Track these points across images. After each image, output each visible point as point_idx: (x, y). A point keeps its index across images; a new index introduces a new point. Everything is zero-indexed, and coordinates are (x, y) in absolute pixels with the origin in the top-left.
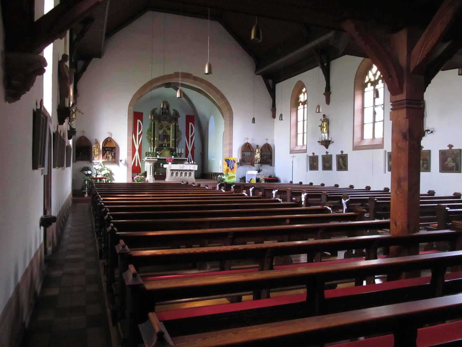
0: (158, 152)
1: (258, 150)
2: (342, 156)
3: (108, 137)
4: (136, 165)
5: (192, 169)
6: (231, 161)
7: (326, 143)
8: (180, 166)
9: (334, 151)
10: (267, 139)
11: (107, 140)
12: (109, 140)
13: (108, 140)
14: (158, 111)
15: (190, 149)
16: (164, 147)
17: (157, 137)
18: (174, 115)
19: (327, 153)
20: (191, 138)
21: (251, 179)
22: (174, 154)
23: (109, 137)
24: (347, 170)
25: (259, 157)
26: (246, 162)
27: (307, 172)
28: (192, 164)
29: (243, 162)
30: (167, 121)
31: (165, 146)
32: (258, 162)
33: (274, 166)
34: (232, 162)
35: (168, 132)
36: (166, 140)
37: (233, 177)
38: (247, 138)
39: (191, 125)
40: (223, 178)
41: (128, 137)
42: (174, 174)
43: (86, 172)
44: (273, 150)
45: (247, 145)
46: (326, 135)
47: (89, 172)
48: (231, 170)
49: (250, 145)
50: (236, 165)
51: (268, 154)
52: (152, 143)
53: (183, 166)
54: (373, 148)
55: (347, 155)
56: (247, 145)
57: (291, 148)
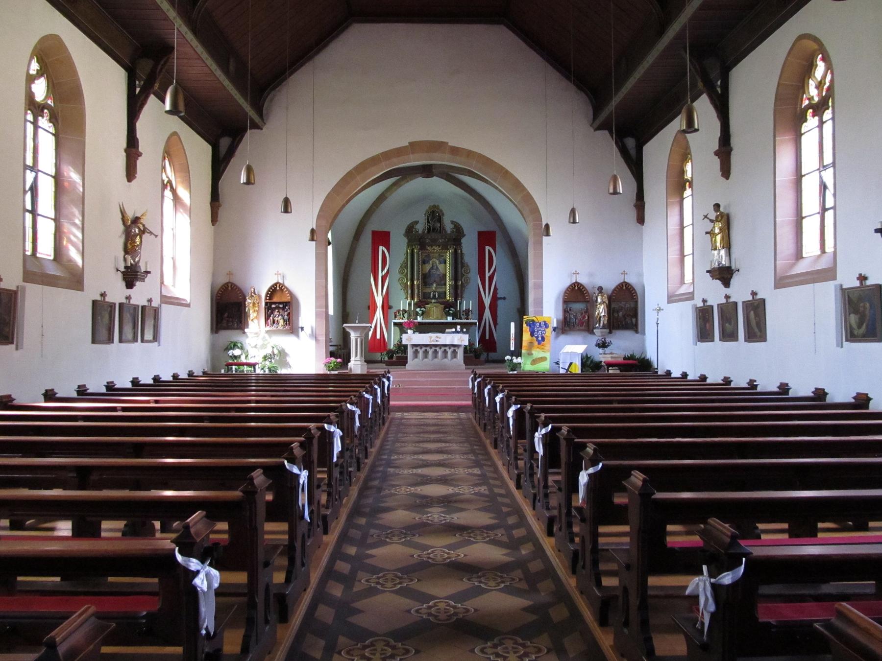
0: (418, 310)
1: (602, 299)
2: (753, 303)
3: (275, 281)
4: (378, 337)
5: (456, 343)
7: (724, 275)
8: (431, 337)
9: (740, 292)
10: (624, 271)
11: (273, 290)
12: (278, 288)
13: (276, 288)
14: (420, 228)
15: (487, 301)
16: (432, 299)
17: (418, 279)
18: (453, 232)
19: (727, 297)
21: (571, 364)
23: (278, 283)
24: (765, 340)
25: (603, 314)
26: (574, 326)
27: (696, 347)
29: (567, 326)
31: (434, 296)
32: (601, 325)
33: (644, 333)
34: (540, 326)
35: (441, 267)
36: (435, 285)
37: (543, 359)
38: (576, 271)
39: (489, 251)
41: (317, 281)
42: (421, 354)
43: (230, 352)
44: (639, 298)
45: (576, 288)
46: (723, 252)
47: (237, 352)
48: (539, 343)
49: (584, 287)
50: (549, 333)
51: (628, 306)
52: (409, 292)
54: (814, 281)
55: (764, 301)
56: (576, 288)
57: (669, 291)
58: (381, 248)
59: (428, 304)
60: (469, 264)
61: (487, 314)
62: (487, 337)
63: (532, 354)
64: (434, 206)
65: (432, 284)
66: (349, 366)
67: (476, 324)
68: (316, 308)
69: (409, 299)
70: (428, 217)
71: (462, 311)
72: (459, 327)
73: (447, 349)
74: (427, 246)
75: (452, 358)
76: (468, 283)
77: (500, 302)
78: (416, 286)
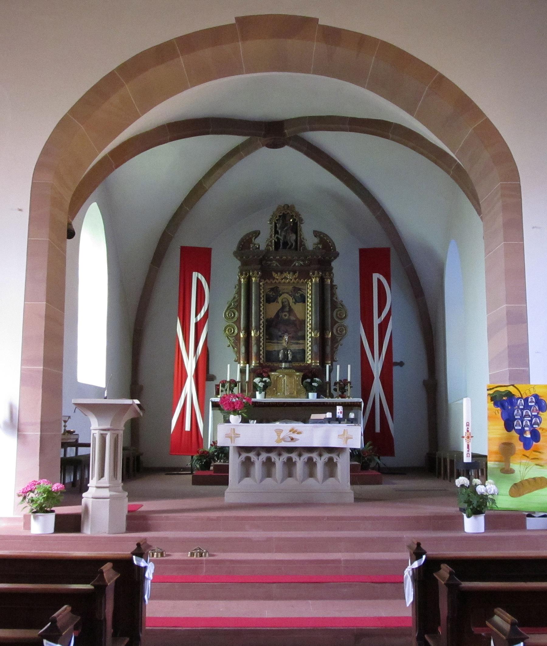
0: (257, 380)
4: (188, 428)
5: (334, 444)
6: (520, 402)
8: (279, 432)
15: (376, 367)
16: (281, 362)
17: (258, 328)
20: (380, 325)
22: (315, 384)
28: (339, 421)
30: (294, 272)
31: (286, 356)
34: (527, 406)
35: (297, 308)
36: (286, 338)
39: (379, 281)
40: (480, 489)
42: (257, 469)
48: (527, 446)
52: (243, 349)
53: (293, 431)
58: (196, 275)
59: (274, 370)
60: (344, 303)
61: (377, 388)
62: (378, 429)
63: (512, 471)
64: (287, 207)
65: (281, 337)
66: (83, 501)
67: (360, 406)
68: (22, 364)
69: (242, 362)
70: (275, 224)
71: (332, 384)
72: (339, 409)
73: (314, 456)
74: (273, 273)
75: (325, 478)
76: (343, 336)
77: (396, 369)
78: (253, 339)
